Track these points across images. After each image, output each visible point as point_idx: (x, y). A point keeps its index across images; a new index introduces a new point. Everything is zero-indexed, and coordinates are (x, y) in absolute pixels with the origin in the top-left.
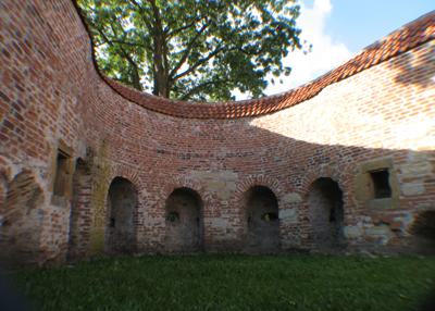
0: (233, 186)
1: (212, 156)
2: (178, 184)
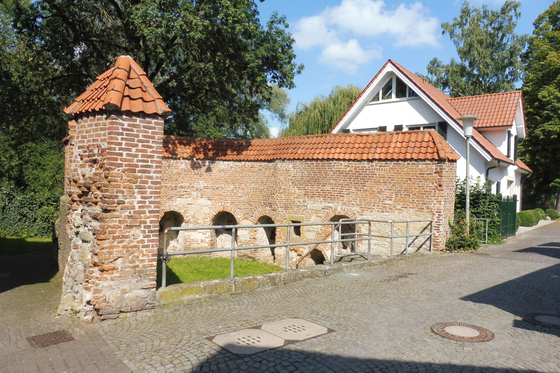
0: (207, 210)
1: (193, 187)
2: (168, 210)
